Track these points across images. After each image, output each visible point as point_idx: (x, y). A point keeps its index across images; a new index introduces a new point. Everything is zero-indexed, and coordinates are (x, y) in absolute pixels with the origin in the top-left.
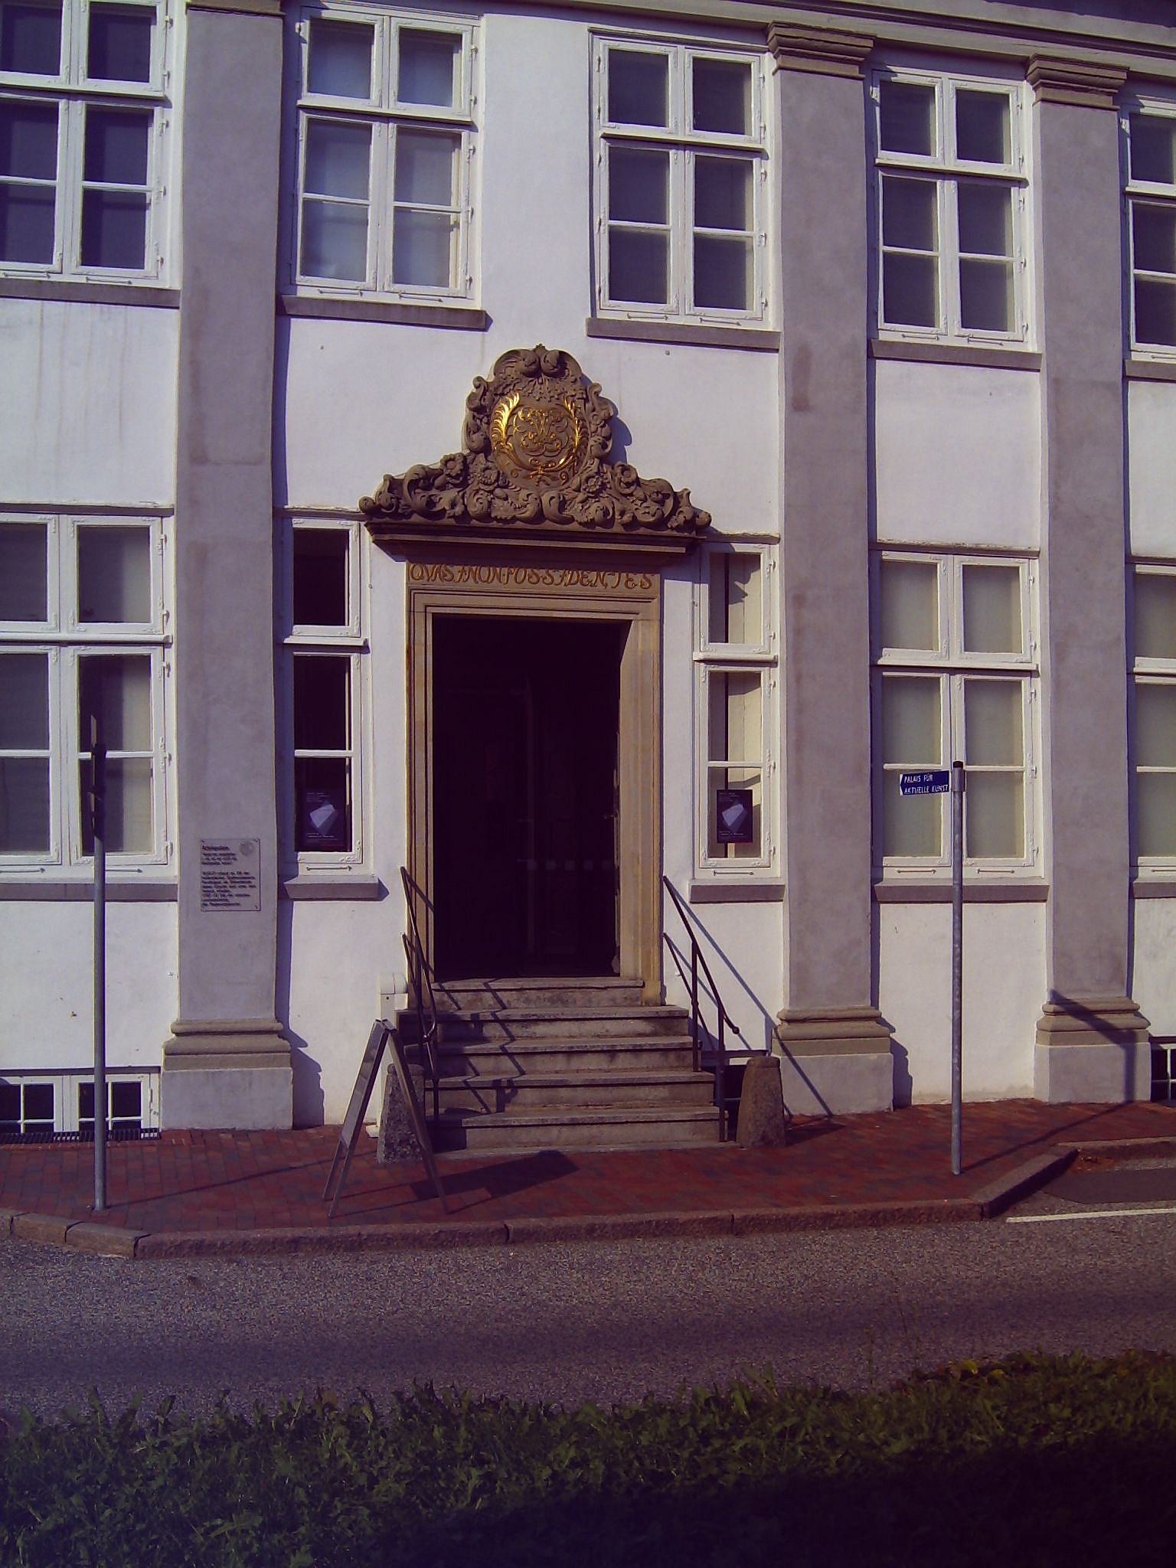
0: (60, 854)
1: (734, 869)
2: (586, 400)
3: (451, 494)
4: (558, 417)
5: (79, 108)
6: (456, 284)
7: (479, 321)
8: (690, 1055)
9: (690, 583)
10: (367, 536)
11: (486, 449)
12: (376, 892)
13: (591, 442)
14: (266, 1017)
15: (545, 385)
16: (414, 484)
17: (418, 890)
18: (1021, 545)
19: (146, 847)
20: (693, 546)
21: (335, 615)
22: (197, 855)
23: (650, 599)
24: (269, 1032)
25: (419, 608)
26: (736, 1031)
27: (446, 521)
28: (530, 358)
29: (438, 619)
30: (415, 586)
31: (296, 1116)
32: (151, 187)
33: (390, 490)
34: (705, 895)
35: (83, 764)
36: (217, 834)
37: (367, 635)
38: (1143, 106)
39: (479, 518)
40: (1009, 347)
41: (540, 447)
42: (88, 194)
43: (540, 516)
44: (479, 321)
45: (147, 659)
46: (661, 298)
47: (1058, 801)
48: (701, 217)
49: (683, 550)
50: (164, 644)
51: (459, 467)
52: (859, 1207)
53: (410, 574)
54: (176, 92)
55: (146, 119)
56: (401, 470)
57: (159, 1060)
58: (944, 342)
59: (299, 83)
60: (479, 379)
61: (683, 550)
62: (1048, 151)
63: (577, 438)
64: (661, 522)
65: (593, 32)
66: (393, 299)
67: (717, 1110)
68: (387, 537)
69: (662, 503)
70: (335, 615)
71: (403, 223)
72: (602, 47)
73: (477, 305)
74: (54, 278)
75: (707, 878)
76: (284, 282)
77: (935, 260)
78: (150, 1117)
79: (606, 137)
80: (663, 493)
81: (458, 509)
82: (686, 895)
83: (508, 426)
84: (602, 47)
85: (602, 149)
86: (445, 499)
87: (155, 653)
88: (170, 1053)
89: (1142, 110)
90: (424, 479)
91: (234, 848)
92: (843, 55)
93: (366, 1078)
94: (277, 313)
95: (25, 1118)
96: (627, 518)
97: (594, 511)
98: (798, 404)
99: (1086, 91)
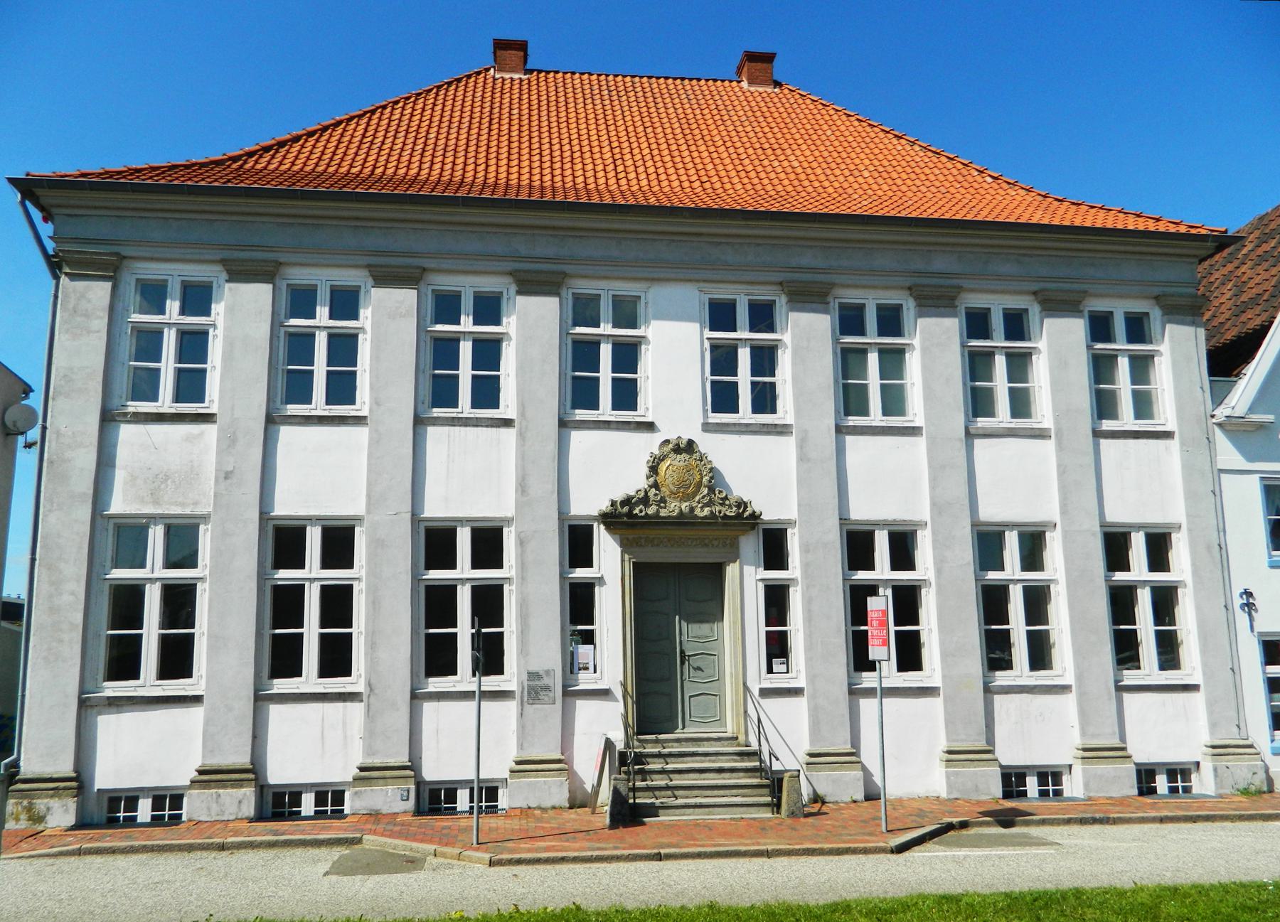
0: (145, 682)
2: (701, 461)
5: (173, 332)
7: (650, 427)
8: (253, 783)
10: (602, 527)
13: (704, 480)
15: (684, 456)
17: (628, 693)
21: (588, 563)
22: (525, 677)
26: (777, 759)
28: (675, 442)
33: (612, 505)
34: (765, 693)
35: (473, 634)
36: (534, 668)
37: (602, 572)
40: (1035, 426)
44: (650, 427)
46: (597, 408)
47: (942, 644)
48: (754, 372)
52: (830, 846)
54: (368, 327)
55: (1030, 354)
56: (619, 497)
57: (506, 775)
58: (874, 424)
67: (770, 799)
69: (739, 508)
70: (588, 563)
73: (649, 420)
74: (460, 415)
75: (767, 685)
77: (1118, 391)
79: (708, 339)
80: (742, 504)
82: (756, 693)
83: (665, 474)
85: (707, 345)
90: (627, 501)
91: (541, 673)
95: (169, 810)
97: (706, 511)
98: (802, 458)
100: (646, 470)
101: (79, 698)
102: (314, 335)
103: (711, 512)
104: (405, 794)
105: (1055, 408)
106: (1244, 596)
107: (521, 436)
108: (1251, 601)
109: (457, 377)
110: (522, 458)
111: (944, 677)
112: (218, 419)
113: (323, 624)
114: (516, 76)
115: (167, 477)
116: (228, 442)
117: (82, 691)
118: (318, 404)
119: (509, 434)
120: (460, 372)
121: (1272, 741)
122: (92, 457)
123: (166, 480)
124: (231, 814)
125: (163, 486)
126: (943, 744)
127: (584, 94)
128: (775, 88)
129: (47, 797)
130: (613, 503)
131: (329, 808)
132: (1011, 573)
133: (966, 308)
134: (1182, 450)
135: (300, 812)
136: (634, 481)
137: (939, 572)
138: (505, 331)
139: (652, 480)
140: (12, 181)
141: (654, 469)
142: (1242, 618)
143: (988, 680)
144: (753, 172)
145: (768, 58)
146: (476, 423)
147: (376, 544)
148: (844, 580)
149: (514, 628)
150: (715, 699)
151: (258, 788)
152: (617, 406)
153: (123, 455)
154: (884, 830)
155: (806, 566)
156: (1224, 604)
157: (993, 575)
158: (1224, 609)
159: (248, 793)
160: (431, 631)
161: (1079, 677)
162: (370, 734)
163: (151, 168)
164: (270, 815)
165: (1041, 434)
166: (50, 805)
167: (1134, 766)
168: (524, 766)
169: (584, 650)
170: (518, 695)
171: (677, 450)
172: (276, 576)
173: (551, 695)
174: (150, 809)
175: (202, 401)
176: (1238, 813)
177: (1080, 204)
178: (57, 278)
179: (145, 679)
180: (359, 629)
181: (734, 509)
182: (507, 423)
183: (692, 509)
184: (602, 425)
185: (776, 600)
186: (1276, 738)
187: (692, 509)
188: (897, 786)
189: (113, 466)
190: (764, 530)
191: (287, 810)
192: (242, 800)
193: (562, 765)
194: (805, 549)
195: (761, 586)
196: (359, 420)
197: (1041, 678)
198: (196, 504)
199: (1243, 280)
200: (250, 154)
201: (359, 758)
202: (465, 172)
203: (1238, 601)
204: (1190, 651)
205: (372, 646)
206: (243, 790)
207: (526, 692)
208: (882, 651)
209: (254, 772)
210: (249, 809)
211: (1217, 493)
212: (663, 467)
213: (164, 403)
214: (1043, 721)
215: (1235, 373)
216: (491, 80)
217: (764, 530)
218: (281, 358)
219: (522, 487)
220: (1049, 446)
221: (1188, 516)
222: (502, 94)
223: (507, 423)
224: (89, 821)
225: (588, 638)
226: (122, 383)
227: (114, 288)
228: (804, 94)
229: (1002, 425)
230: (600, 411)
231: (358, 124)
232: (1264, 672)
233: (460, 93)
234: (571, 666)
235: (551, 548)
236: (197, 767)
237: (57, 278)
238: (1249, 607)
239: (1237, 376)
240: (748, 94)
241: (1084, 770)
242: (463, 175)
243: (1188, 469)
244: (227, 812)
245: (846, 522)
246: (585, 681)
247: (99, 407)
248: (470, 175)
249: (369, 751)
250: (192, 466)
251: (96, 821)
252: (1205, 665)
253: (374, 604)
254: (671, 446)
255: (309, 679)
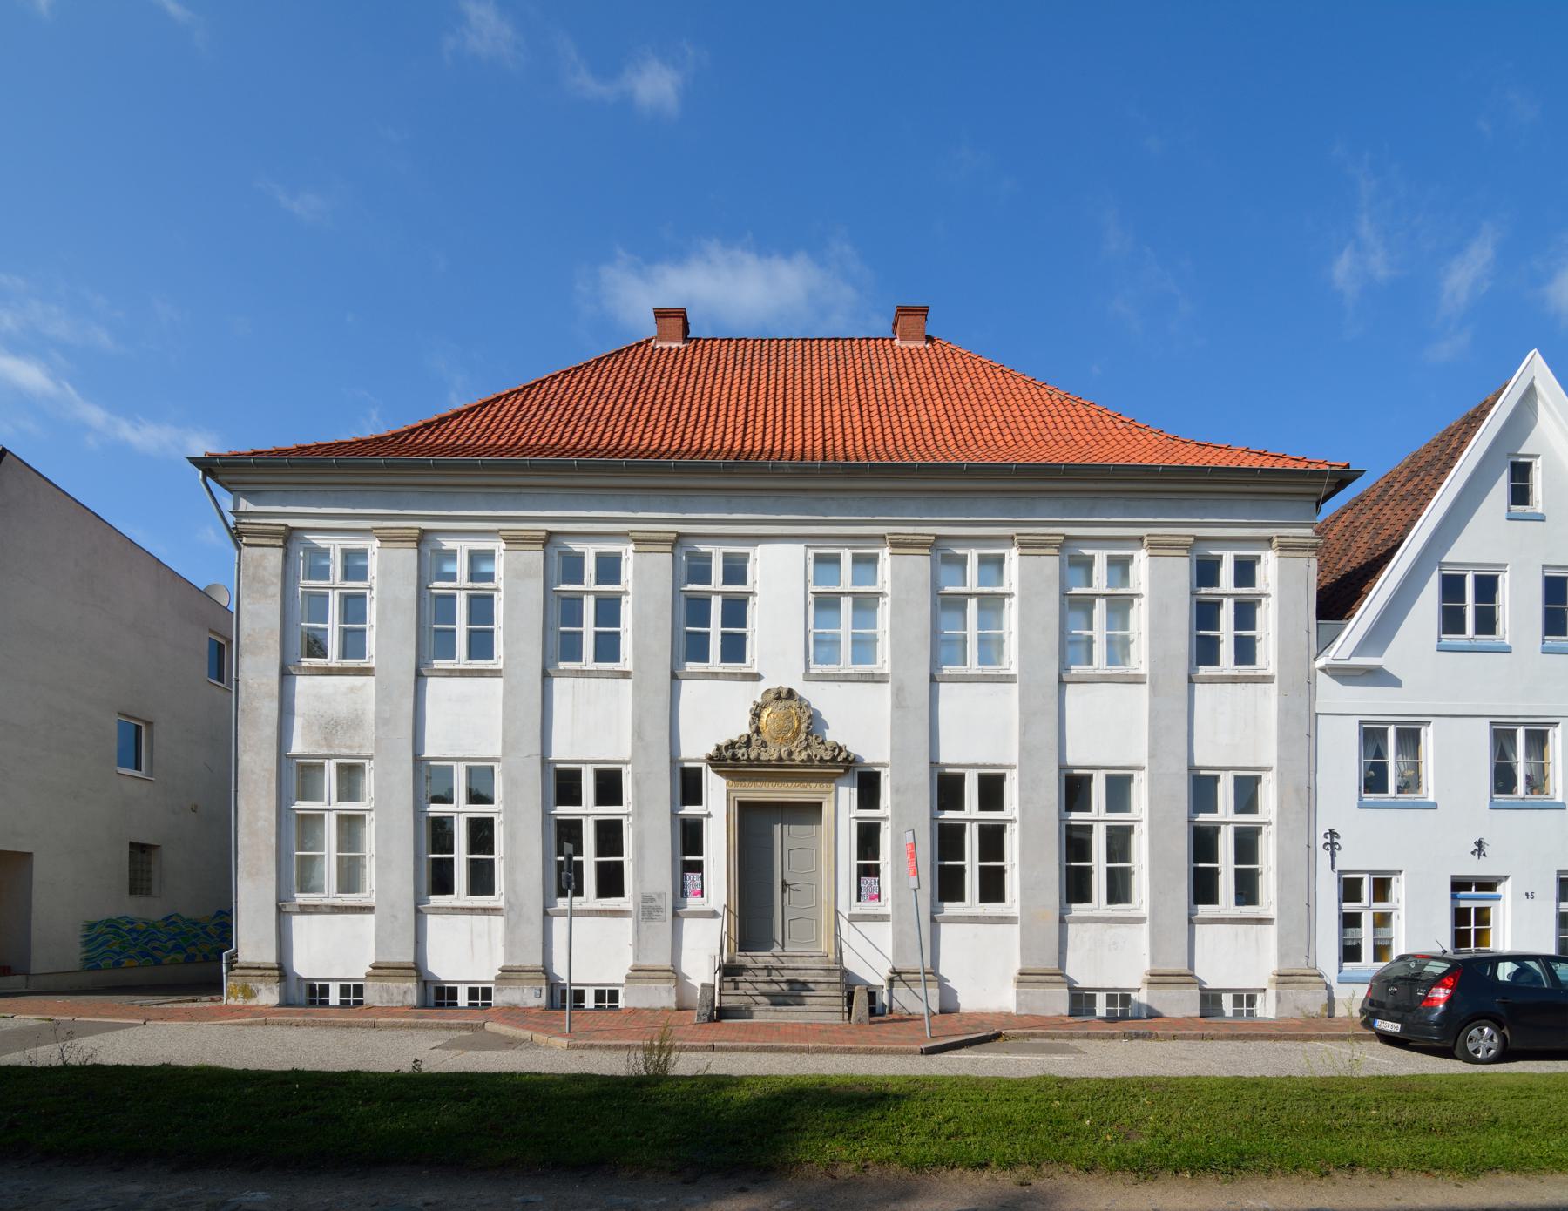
1: (868, 907)
2: (801, 708)
3: (744, 750)
4: (788, 717)
6: (1005, 664)
7: (756, 677)
9: (848, 788)
10: (710, 768)
11: (758, 731)
12: (714, 915)
14: (1184, 968)
15: (783, 704)
16: (727, 747)
17: (731, 912)
18: (1006, 763)
19: (364, 891)
20: (847, 770)
22: (640, 899)
23: (830, 792)
24: (669, 971)
25: (732, 798)
27: (797, 763)
29: (740, 803)
30: (733, 788)
31: (677, 1002)
32: (1005, 630)
34: (853, 919)
38: (445, 545)
39: (755, 760)
41: (781, 729)
42: (1237, 638)
43: (780, 758)
44: (756, 677)
45: (364, 816)
46: (707, 660)
47: (1022, 878)
49: (842, 771)
50: (627, 815)
51: (746, 739)
53: (728, 784)
56: (723, 742)
57: (623, 980)
59: (299, 577)
60: (755, 702)
61: (842, 771)
62: (1023, 579)
63: (796, 724)
64: (834, 759)
65: (807, 547)
66: (721, 670)
68: (716, 769)
69: (834, 750)
71: (983, 641)
72: (811, 552)
73: (755, 671)
74: (584, 668)
76: (1064, 667)
78: (621, 1004)
81: (746, 757)
83: (767, 721)
84: (811, 552)
85: (811, 598)
86: (740, 753)
87: (367, 813)
88: (628, 978)
89: (444, 548)
90: (732, 745)
91: (655, 896)
92: (921, 545)
93: (26, 988)
94: (931, 681)
96: (818, 758)
97: (804, 756)
99: (1043, 548)
100: (749, 717)
101: (277, 905)
102: (582, 599)
103: (809, 756)
104: (538, 992)
105: (1152, 656)
106: (1329, 836)
107: (636, 688)
108: (1335, 840)
109: (581, 633)
110: (637, 705)
111: (1022, 908)
112: (375, 672)
113: (599, 854)
114: (674, 345)
115: (336, 724)
116: (383, 696)
117: (279, 900)
118: (461, 660)
119: (627, 684)
120: (457, 626)
121: (1340, 971)
122: (275, 705)
123: (337, 726)
124: (397, 1002)
125: (334, 732)
126: (1017, 966)
127: (913, 359)
128: (926, 343)
129: (256, 981)
130: (718, 748)
131: (480, 1002)
132: (1096, 813)
133: (1197, 556)
134: (1279, 695)
135: (583, 1006)
136: (739, 727)
137: (1023, 811)
138: (623, 590)
139: (754, 726)
140: (196, 462)
141: (756, 715)
142: (1324, 857)
143: (1063, 911)
144: (1101, 423)
145: (923, 312)
146: (598, 674)
147: (511, 783)
148: (1060, 820)
149: (889, 859)
150: (812, 924)
151: (421, 984)
152: (726, 657)
153: (300, 704)
154: (928, 1036)
155: (896, 806)
156: (1307, 843)
157: (1203, 817)
158: (1306, 849)
159: (411, 986)
160: (688, 858)
161: (1153, 910)
162: (510, 943)
163: (318, 445)
164: (433, 1005)
165: (1137, 680)
166: (260, 987)
167: (1198, 991)
168: (639, 974)
169: (692, 877)
170: (634, 914)
171: (778, 698)
172: (428, 810)
173: (663, 914)
174: (594, 1000)
175: (364, 657)
176: (1029, 1031)
177: (1206, 446)
178: (239, 548)
179: (329, 891)
180: (499, 855)
181: (830, 752)
182: (625, 675)
183: (790, 753)
184: (710, 677)
185: (868, 838)
186: (1344, 969)
187: (790, 753)
188: (970, 1000)
189: (293, 714)
190: (859, 773)
191: (318, 998)
192: (407, 992)
193: (674, 973)
194: (896, 790)
195: (854, 823)
196: (495, 673)
197: (1119, 910)
198: (361, 746)
199: (1382, 522)
200: (412, 431)
201: (500, 962)
202: (793, 440)
203: (1321, 841)
204: (1268, 886)
205: (510, 871)
206: (408, 984)
207: (641, 913)
208: (1226, 885)
209: (417, 968)
210: (413, 998)
211: (1312, 736)
212: (765, 715)
213: (332, 659)
214: (1115, 949)
215: (1347, 615)
216: (651, 350)
217: (859, 773)
218: (682, 621)
219: (638, 733)
220: (1144, 691)
221: (1279, 758)
222: (778, 356)
223: (625, 675)
224: (292, 1002)
225: (697, 867)
226: (297, 644)
227: (286, 556)
228: (954, 348)
229: (1097, 672)
230: (711, 663)
231: (516, 399)
232: (1340, 908)
233: (617, 366)
234: (681, 892)
235: (662, 788)
236: (500, 966)
237: (239, 548)
238: (1333, 847)
239: (1348, 619)
240: (898, 351)
241: (1148, 993)
242: (793, 444)
243: (1284, 713)
244: (395, 1001)
245: (935, 766)
246: (693, 903)
247: (278, 662)
248: (728, 443)
249: (509, 953)
250: (357, 714)
251: (297, 1001)
252: (1280, 901)
253: (511, 836)
254: (772, 696)
255: (460, 894)
